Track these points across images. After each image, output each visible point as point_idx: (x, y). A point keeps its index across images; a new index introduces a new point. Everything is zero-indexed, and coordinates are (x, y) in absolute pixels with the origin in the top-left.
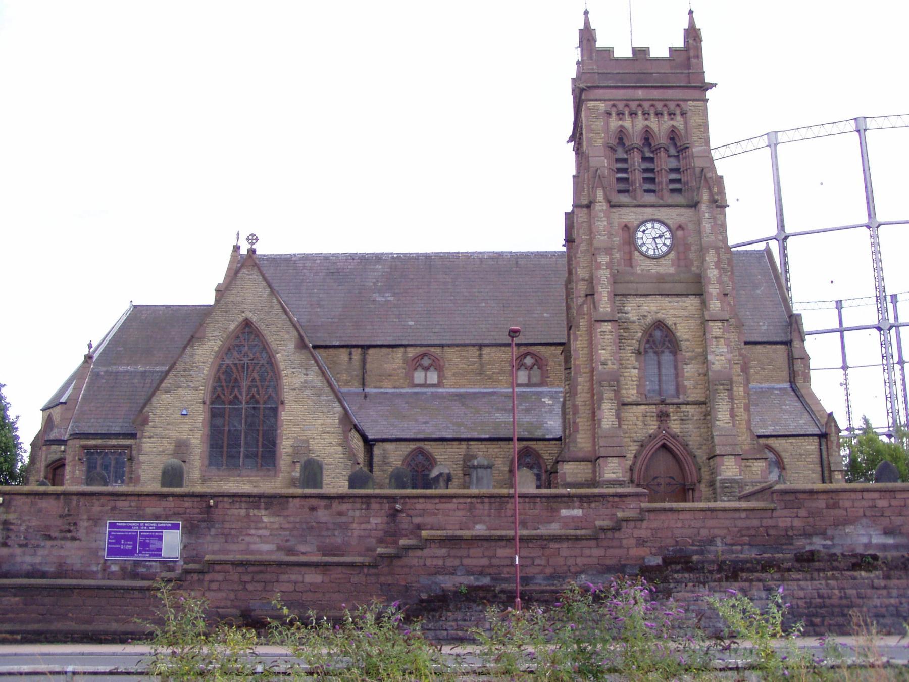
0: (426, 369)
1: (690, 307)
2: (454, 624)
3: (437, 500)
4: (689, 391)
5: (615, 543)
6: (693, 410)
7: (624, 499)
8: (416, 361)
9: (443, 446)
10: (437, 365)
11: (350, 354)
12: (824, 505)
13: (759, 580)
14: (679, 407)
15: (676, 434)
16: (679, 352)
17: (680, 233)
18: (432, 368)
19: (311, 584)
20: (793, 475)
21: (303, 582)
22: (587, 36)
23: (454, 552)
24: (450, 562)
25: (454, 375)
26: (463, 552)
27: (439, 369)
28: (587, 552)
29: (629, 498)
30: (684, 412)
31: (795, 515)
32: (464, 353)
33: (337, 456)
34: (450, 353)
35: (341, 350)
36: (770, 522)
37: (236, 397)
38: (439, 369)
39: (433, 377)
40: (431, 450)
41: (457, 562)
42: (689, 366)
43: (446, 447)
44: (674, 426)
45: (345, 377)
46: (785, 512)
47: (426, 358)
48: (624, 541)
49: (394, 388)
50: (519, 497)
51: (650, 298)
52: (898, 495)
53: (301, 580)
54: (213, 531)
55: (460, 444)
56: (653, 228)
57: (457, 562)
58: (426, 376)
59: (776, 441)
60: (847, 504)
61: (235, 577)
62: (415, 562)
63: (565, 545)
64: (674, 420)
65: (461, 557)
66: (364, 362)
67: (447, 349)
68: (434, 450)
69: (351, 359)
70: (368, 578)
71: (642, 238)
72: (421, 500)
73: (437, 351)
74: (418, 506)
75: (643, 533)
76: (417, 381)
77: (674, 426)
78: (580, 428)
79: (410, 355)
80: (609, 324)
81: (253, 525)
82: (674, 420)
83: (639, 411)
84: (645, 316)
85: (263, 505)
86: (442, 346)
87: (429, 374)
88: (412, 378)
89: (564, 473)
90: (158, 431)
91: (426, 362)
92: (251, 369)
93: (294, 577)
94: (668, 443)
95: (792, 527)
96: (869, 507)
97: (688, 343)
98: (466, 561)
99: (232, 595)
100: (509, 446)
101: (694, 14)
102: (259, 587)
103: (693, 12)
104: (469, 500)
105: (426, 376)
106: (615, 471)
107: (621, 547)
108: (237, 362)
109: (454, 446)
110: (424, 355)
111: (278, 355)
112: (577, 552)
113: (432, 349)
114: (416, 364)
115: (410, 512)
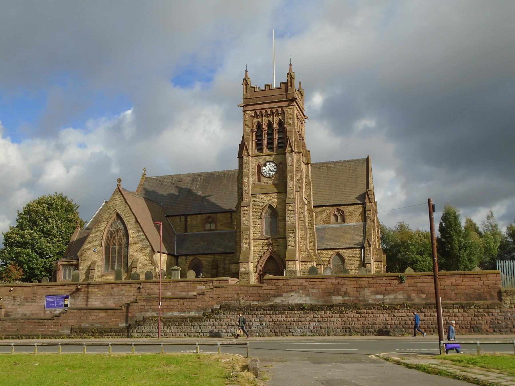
0: (210, 223)
1: (283, 198)
2: (147, 330)
3: (154, 284)
4: (281, 233)
5: (203, 300)
6: (282, 241)
7: (220, 282)
8: (206, 219)
9: (204, 257)
10: (214, 221)
11: (180, 218)
12: (283, 285)
13: (255, 314)
14: (277, 240)
15: (275, 251)
16: (278, 217)
17: (281, 166)
18: (213, 223)
19: (101, 316)
20: (349, 265)
21: (99, 316)
22: (246, 82)
23: (148, 304)
24: (146, 308)
25: (221, 225)
26: (151, 304)
27: (215, 223)
28: (193, 303)
29: (222, 281)
30: (279, 242)
31: (271, 289)
32: (225, 216)
33: (149, 264)
34: (220, 216)
35: (177, 217)
36: (261, 292)
37: (114, 243)
38: (215, 223)
39: (213, 227)
40: (200, 259)
41: (149, 307)
42: (281, 223)
43: (206, 257)
44: (275, 248)
45: (178, 228)
46: (267, 288)
47: (210, 219)
48: (207, 299)
49: (197, 232)
50: (161, 282)
51: (266, 195)
52: (312, 280)
53: (98, 315)
54: (80, 298)
55: (211, 256)
56: (269, 164)
57: (149, 307)
58: (210, 226)
59: (342, 250)
60: (292, 284)
61: (77, 315)
62: (135, 308)
63: (186, 300)
64: (275, 246)
65: (150, 306)
66: (186, 221)
67: (218, 214)
68: (202, 259)
69: (180, 220)
70: (120, 314)
71: (265, 169)
72: (149, 284)
73: (214, 215)
74: (148, 286)
75: (213, 296)
76: (207, 228)
77: (275, 248)
78: (238, 250)
79: (204, 217)
80: (247, 207)
81: (93, 295)
82: (275, 246)
83: (261, 242)
84: (264, 202)
85: (96, 287)
86: (216, 213)
87: (211, 225)
88: (205, 227)
89: (232, 269)
90: (86, 258)
91: (210, 220)
92: (119, 232)
93: (96, 314)
94: (272, 255)
95: (269, 294)
96: (300, 285)
97: (281, 213)
98: (152, 307)
99: (76, 321)
100: (230, 256)
101: (292, 66)
102: (85, 318)
103: (291, 65)
104: (165, 283)
105: (210, 226)
106: (245, 268)
107: (205, 301)
108: (114, 229)
109: (209, 257)
110: (209, 218)
111: (128, 226)
112: (190, 303)
113: (212, 215)
114: (207, 221)
115: (146, 288)
